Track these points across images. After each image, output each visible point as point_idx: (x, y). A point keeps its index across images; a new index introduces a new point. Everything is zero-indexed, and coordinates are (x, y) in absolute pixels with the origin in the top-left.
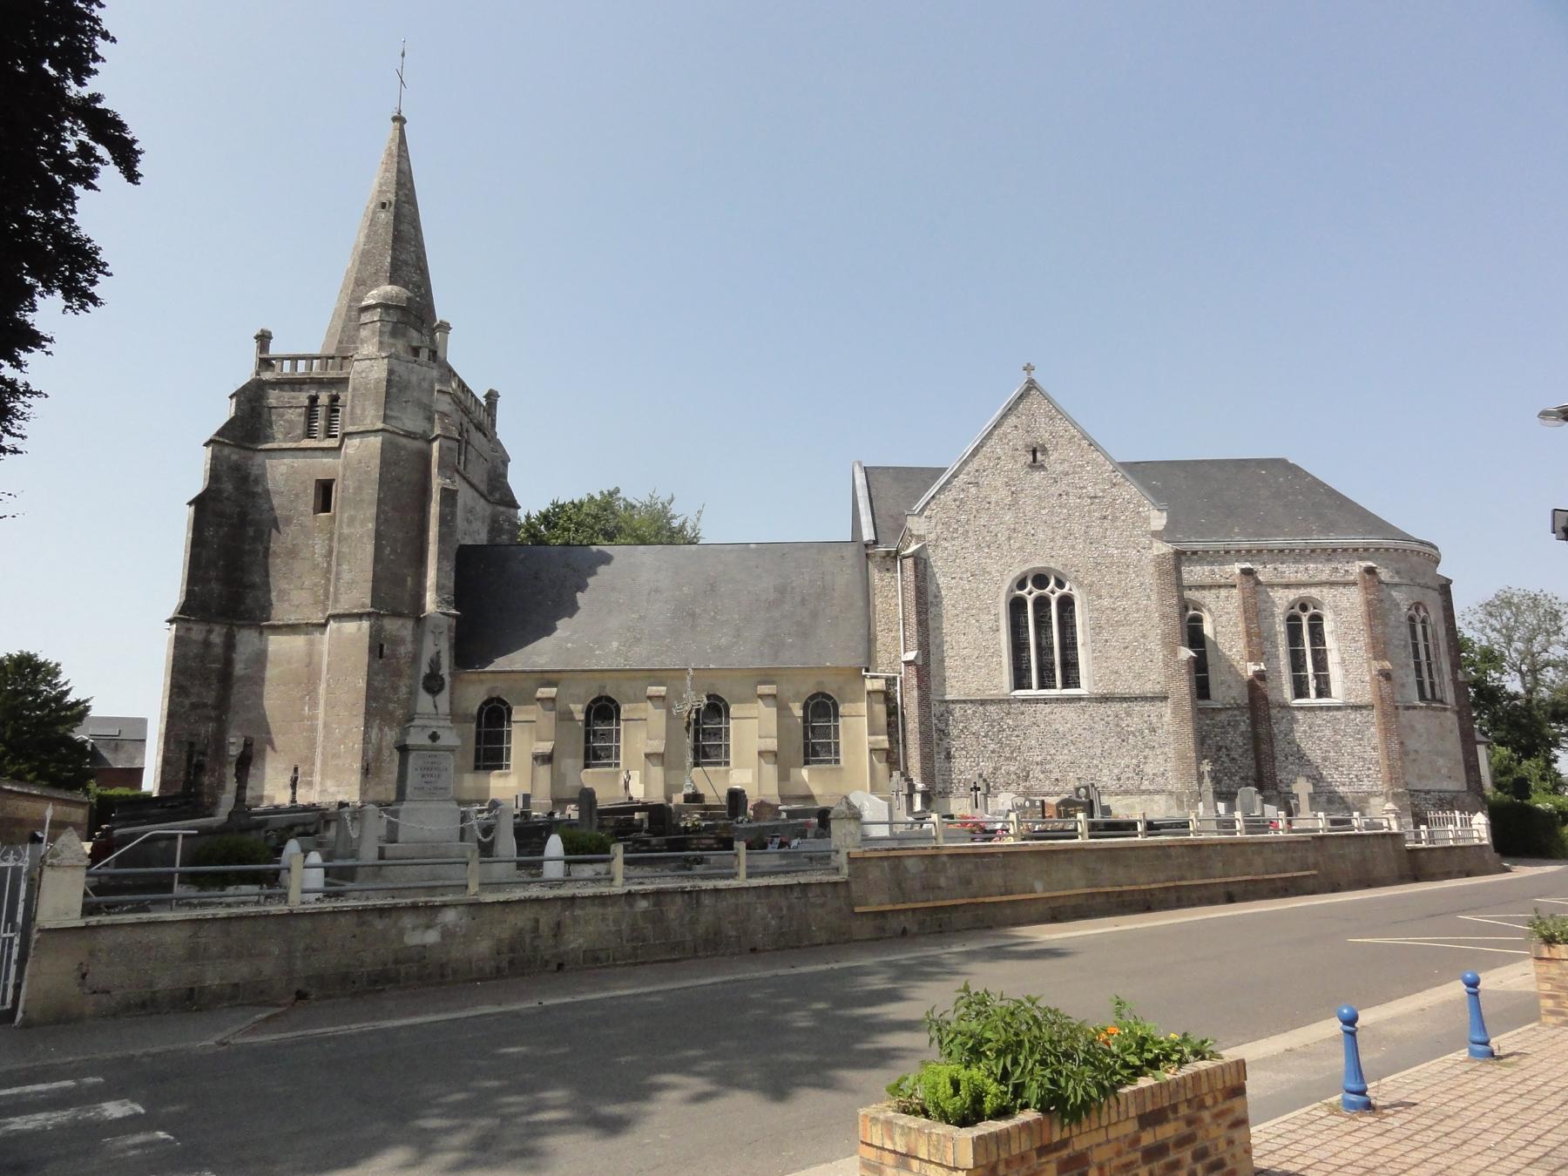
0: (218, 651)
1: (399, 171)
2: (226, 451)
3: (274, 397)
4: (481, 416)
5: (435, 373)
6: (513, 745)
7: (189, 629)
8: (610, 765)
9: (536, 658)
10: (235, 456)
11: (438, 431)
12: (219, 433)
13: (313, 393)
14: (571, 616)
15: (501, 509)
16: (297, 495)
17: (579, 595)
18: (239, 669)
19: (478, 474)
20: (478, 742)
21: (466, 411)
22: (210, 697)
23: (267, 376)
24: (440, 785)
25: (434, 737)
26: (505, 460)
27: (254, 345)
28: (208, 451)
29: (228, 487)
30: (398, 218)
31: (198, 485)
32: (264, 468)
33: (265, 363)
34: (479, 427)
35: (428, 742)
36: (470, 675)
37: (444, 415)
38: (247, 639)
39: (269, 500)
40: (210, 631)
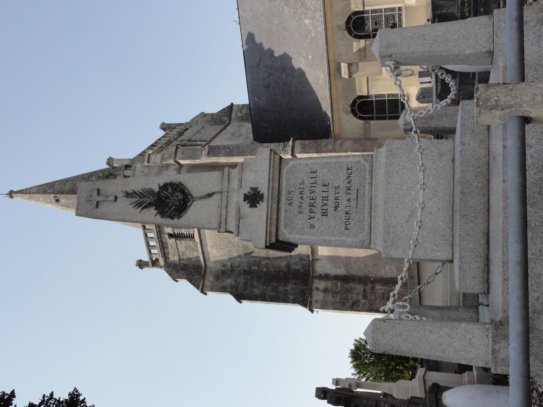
0: (329, 284)
1: (37, 193)
2: (207, 283)
3: (173, 258)
4: (175, 132)
5: (138, 165)
6: (386, 93)
7: (316, 301)
8: (400, 15)
9: (321, 82)
10: (209, 279)
11: (172, 162)
12: (198, 288)
13: (167, 236)
14: (291, 58)
15: (233, 115)
16: (229, 243)
17: (276, 55)
18: (341, 271)
19: (212, 131)
20: (384, 118)
21: (169, 143)
22: (359, 288)
23: (162, 262)
24: (341, 182)
25: (253, 198)
26: (203, 115)
27: (146, 270)
28: (210, 293)
29: (229, 282)
30: (62, 192)
31: (229, 298)
32: (215, 262)
33: (155, 263)
34: (181, 134)
35: (263, 207)
36: (336, 129)
37: (163, 159)
38: (320, 268)
39: (235, 258)
40: (317, 289)
